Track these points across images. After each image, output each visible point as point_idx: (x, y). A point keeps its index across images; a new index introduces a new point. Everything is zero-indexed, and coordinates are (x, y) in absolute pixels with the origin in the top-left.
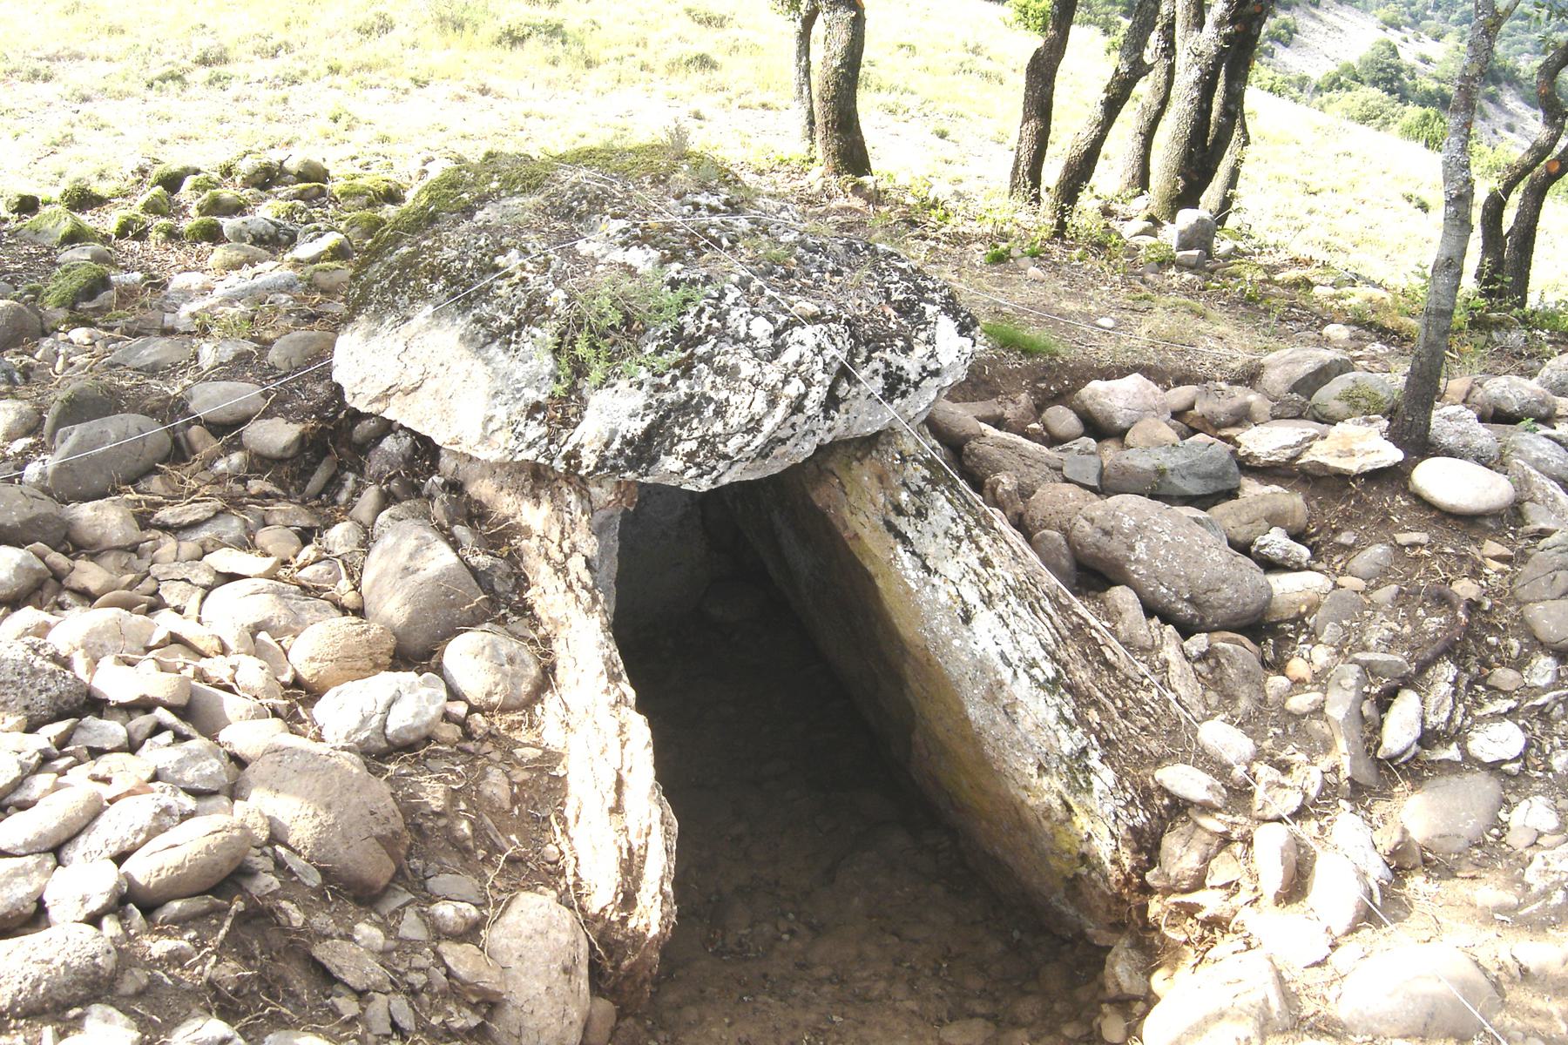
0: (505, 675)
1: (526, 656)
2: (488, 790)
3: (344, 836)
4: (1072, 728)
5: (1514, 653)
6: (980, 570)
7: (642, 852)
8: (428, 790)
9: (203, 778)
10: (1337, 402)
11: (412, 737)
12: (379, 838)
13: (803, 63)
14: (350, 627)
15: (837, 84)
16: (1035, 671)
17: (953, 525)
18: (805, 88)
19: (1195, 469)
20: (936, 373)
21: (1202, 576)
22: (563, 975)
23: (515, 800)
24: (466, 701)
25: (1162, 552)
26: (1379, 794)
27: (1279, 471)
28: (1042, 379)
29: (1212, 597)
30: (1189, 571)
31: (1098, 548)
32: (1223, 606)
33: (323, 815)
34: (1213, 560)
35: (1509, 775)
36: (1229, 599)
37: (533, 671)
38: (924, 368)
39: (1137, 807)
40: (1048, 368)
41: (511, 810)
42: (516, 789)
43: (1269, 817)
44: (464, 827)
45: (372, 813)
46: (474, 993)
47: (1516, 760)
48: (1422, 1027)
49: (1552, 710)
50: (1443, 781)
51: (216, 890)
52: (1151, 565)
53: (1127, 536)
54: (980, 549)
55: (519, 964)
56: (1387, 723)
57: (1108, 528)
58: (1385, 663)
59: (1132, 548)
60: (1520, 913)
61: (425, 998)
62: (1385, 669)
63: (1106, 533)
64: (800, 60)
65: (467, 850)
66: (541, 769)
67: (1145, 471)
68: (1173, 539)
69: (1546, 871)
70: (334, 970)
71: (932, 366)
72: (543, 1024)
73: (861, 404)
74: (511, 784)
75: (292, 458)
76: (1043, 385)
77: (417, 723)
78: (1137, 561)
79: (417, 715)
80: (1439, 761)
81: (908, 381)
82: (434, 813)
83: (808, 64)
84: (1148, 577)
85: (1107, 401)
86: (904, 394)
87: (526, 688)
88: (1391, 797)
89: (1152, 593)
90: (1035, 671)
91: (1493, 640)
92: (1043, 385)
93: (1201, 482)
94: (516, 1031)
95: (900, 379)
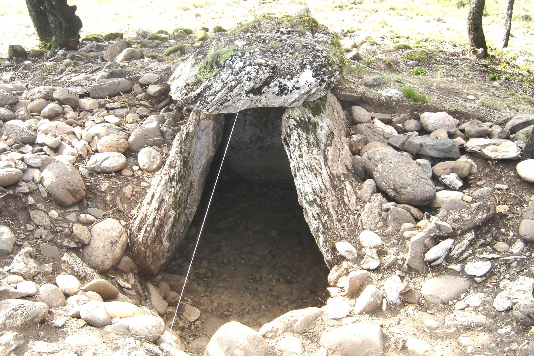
0: (150, 161)
1: (158, 157)
2: (124, 190)
3: (57, 186)
4: (315, 220)
5: (510, 237)
6: (298, 158)
7: (148, 217)
8: (104, 185)
9: (34, 163)
10: (522, 135)
11: (108, 170)
12: (69, 190)
13: (509, 13)
14: (114, 139)
15: (474, 14)
16: (307, 197)
17: (295, 142)
18: (509, 22)
19: (435, 147)
20: (298, 88)
21: (399, 181)
22: (110, 244)
23: (133, 196)
24: (139, 167)
25: (387, 170)
26: (420, 274)
27: (476, 155)
28: (416, 110)
29: (403, 190)
30: (395, 178)
31: (366, 164)
32: (406, 195)
33: (54, 179)
34: (407, 177)
35: (475, 282)
36: (409, 192)
37: (158, 162)
38: (294, 86)
39: (329, 254)
40: (420, 107)
41: (130, 198)
42: (134, 193)
43: (364, 268)
44: (108, 198)
45: (68, 182)
46: (77, 239)
47: (481, 277)
48: (335, 347)
49: (511, 263)
50: (447, 276)
51: (5, 187)
52: (382, 173)
53: (376, 161)
54: (301, 151)
55: (97, 236)
56: (432, 249)
57: (370, 157)
58: (444, 226)
59: (376, 166)
60: (436, 331)
61: (59, 234)
62: (444, 229)
63: (370, 159)
64: (508, 11)
65: (107, 204)
66: (144, 189)
67: (416, 144)
68: (394, 166)
69: (454, 319)
70: (32, 217)
71: (297, 86)
72: (98, 255)
73: (270, 95)
74: (133, 191)
75: (157, 97)
76: (416, 113)
77: (110, 166)
78: (377, 171)
79: (110, 164)
80: (450, 269)
81: (288, 90)
82: (102, 192)
83: (511, 13)
84: (380, 177)
85: (427, 120)
86: (286, 94)
87: (155, 166)
88: (425, 277)
89: (380, 184)
90: (307, 197)
91: (503, 230)
92: (416, 113)
93: (438, 152)
94: (90, 254)
95: (285, 89)
